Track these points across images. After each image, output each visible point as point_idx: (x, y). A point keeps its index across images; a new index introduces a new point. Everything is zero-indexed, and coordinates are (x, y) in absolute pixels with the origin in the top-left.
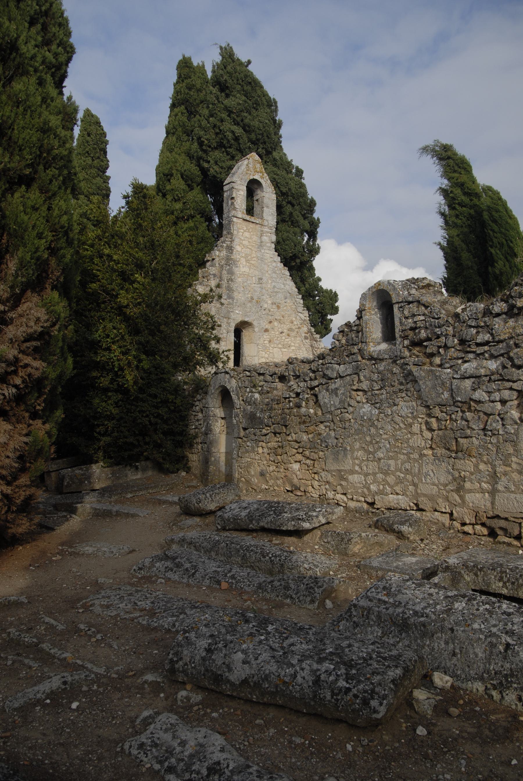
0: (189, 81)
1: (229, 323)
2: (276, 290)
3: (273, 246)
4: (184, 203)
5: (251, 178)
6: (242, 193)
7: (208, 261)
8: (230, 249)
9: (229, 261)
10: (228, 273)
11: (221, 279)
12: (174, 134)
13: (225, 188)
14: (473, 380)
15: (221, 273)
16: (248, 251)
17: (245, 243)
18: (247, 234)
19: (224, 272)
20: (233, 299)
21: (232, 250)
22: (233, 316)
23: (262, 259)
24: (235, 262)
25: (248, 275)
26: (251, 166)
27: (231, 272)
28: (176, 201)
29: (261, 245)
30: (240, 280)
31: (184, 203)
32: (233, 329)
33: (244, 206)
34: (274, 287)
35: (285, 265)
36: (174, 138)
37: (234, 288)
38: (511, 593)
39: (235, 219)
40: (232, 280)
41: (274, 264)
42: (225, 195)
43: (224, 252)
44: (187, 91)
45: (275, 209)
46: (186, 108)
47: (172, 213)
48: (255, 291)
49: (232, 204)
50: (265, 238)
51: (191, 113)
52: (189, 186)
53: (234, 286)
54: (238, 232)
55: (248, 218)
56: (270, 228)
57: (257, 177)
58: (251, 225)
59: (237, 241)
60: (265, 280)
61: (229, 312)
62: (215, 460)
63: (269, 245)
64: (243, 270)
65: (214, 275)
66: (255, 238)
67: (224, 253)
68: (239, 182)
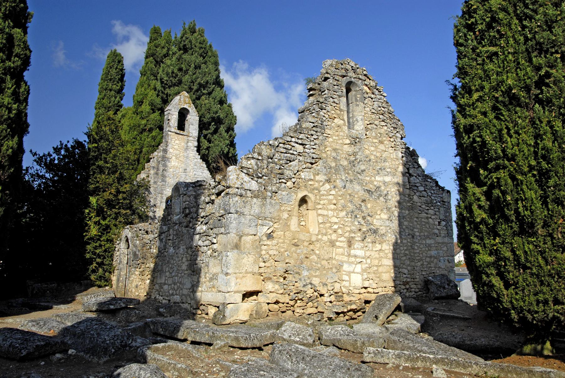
0: (157, 41)
1: (162, 197)
2: (196, 176)
3: (196, 149)
4: (148, 120)
5: (182, 107)
6: (175, 116)
7: (151, 158)
8: (165, 151)
9: (164, 159)
10: (163, 166)
11: (158, 169)
12: (145, 75)
13: (166, 113)
14: (224, 323)
15: (158, 166)
16: (178, 152)
17: (176, 147)
18: (177, 142)
19: (160, 165)
20: (165, 182)
21: (167, 152)
22: (165, 192)
23: (187, 157)
24: (168, 159)
25: (177, 167)
26: (182, 99)
27: (165, 165)
28: (143, 118)
29: (187, 148)
30: (171, 170)
31: (148, 120)
32: (164, 200)
33: (176, 124)
34: (195, 174)
35: (203, 161)
36: (145, 78)
37: (167, 175)
38: (346, 113)
39: (169, 133)
40: (166, 170)
41: (196, 160)
42: (166, 117)
43: (161, 153)
44: (154, 48)
45: (198, 126)
46: (154, 59)
47: (139, 126)
48: (181, 177)
49: (168, 123)
50: (190, 144)
51: (158, 63)
52: (152, 109)
53: (166, 174)
54: (171, 140)
55: (178, 132)
56: (194, 138)
57: (186, 106)
58: (181, 136)
59: (170, 146)
60: (188, 170)
61: (162, 190)
62: (39, 365)
63: (192, 148)
64: (173, 164)
65: (154, 167)
66: (183, 144)
67: (161, 154)
68: (173, 110)
